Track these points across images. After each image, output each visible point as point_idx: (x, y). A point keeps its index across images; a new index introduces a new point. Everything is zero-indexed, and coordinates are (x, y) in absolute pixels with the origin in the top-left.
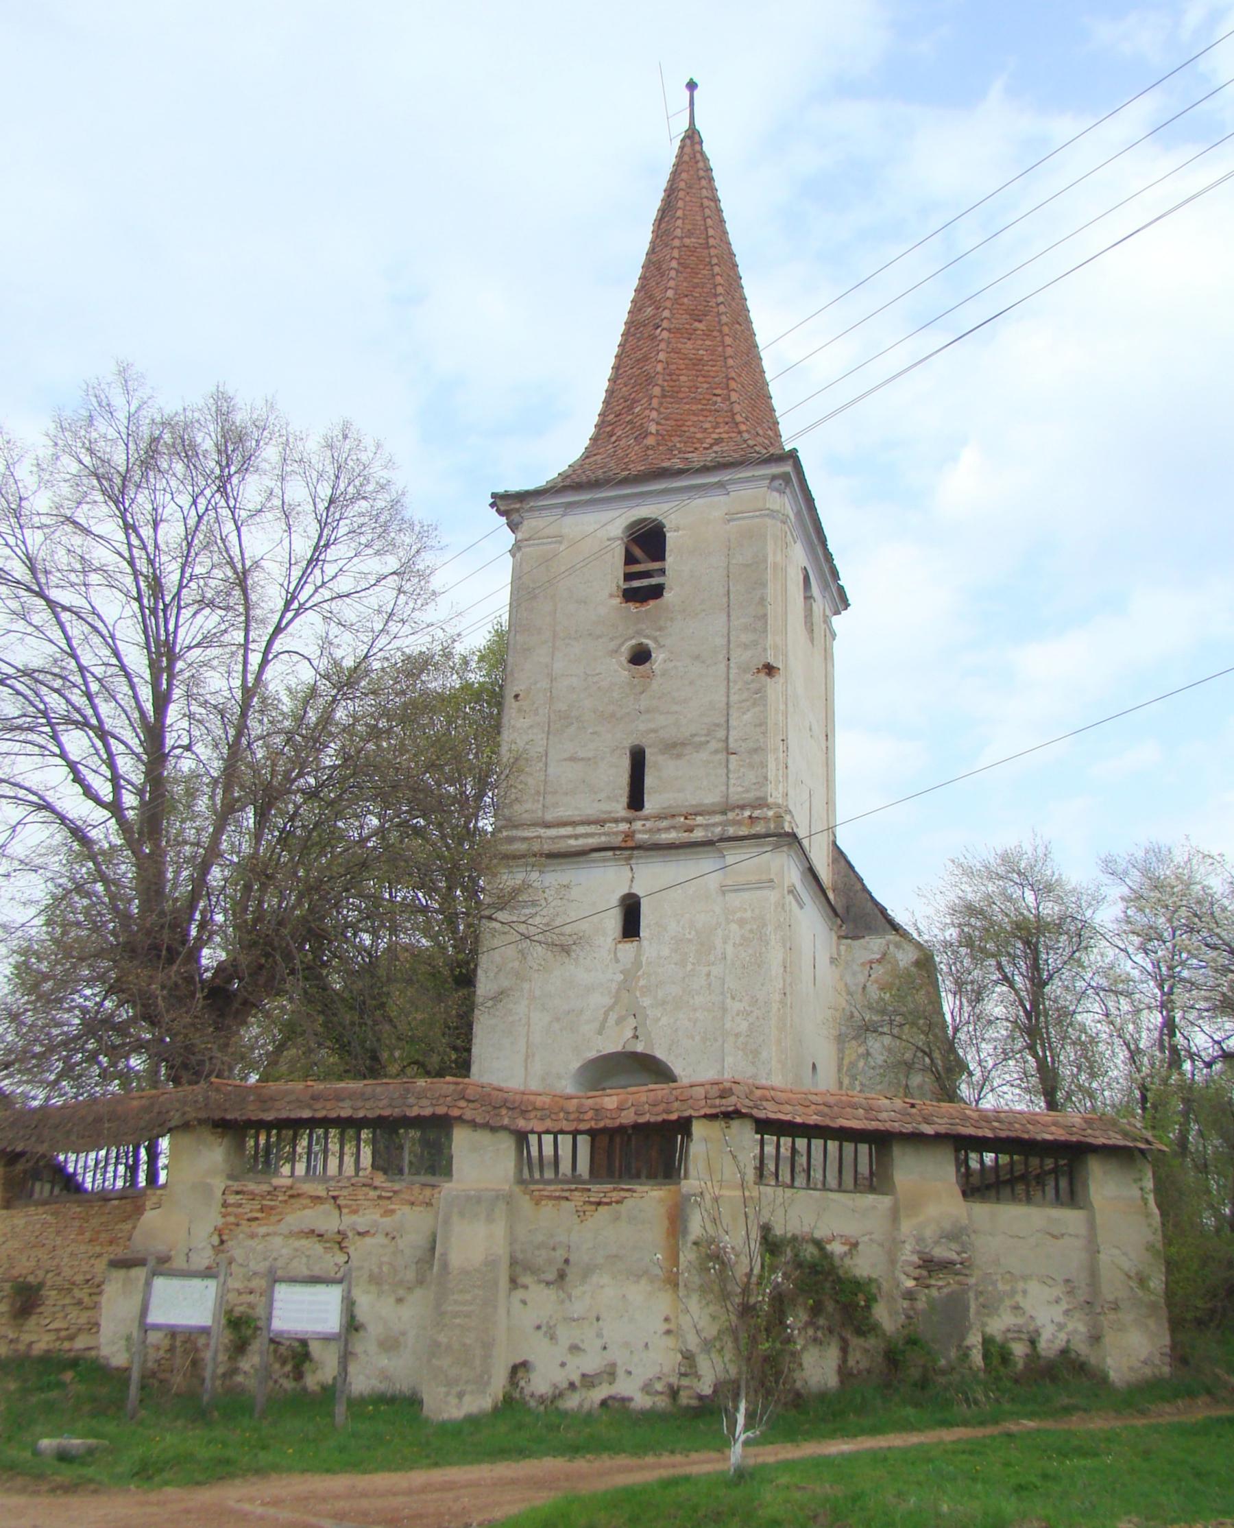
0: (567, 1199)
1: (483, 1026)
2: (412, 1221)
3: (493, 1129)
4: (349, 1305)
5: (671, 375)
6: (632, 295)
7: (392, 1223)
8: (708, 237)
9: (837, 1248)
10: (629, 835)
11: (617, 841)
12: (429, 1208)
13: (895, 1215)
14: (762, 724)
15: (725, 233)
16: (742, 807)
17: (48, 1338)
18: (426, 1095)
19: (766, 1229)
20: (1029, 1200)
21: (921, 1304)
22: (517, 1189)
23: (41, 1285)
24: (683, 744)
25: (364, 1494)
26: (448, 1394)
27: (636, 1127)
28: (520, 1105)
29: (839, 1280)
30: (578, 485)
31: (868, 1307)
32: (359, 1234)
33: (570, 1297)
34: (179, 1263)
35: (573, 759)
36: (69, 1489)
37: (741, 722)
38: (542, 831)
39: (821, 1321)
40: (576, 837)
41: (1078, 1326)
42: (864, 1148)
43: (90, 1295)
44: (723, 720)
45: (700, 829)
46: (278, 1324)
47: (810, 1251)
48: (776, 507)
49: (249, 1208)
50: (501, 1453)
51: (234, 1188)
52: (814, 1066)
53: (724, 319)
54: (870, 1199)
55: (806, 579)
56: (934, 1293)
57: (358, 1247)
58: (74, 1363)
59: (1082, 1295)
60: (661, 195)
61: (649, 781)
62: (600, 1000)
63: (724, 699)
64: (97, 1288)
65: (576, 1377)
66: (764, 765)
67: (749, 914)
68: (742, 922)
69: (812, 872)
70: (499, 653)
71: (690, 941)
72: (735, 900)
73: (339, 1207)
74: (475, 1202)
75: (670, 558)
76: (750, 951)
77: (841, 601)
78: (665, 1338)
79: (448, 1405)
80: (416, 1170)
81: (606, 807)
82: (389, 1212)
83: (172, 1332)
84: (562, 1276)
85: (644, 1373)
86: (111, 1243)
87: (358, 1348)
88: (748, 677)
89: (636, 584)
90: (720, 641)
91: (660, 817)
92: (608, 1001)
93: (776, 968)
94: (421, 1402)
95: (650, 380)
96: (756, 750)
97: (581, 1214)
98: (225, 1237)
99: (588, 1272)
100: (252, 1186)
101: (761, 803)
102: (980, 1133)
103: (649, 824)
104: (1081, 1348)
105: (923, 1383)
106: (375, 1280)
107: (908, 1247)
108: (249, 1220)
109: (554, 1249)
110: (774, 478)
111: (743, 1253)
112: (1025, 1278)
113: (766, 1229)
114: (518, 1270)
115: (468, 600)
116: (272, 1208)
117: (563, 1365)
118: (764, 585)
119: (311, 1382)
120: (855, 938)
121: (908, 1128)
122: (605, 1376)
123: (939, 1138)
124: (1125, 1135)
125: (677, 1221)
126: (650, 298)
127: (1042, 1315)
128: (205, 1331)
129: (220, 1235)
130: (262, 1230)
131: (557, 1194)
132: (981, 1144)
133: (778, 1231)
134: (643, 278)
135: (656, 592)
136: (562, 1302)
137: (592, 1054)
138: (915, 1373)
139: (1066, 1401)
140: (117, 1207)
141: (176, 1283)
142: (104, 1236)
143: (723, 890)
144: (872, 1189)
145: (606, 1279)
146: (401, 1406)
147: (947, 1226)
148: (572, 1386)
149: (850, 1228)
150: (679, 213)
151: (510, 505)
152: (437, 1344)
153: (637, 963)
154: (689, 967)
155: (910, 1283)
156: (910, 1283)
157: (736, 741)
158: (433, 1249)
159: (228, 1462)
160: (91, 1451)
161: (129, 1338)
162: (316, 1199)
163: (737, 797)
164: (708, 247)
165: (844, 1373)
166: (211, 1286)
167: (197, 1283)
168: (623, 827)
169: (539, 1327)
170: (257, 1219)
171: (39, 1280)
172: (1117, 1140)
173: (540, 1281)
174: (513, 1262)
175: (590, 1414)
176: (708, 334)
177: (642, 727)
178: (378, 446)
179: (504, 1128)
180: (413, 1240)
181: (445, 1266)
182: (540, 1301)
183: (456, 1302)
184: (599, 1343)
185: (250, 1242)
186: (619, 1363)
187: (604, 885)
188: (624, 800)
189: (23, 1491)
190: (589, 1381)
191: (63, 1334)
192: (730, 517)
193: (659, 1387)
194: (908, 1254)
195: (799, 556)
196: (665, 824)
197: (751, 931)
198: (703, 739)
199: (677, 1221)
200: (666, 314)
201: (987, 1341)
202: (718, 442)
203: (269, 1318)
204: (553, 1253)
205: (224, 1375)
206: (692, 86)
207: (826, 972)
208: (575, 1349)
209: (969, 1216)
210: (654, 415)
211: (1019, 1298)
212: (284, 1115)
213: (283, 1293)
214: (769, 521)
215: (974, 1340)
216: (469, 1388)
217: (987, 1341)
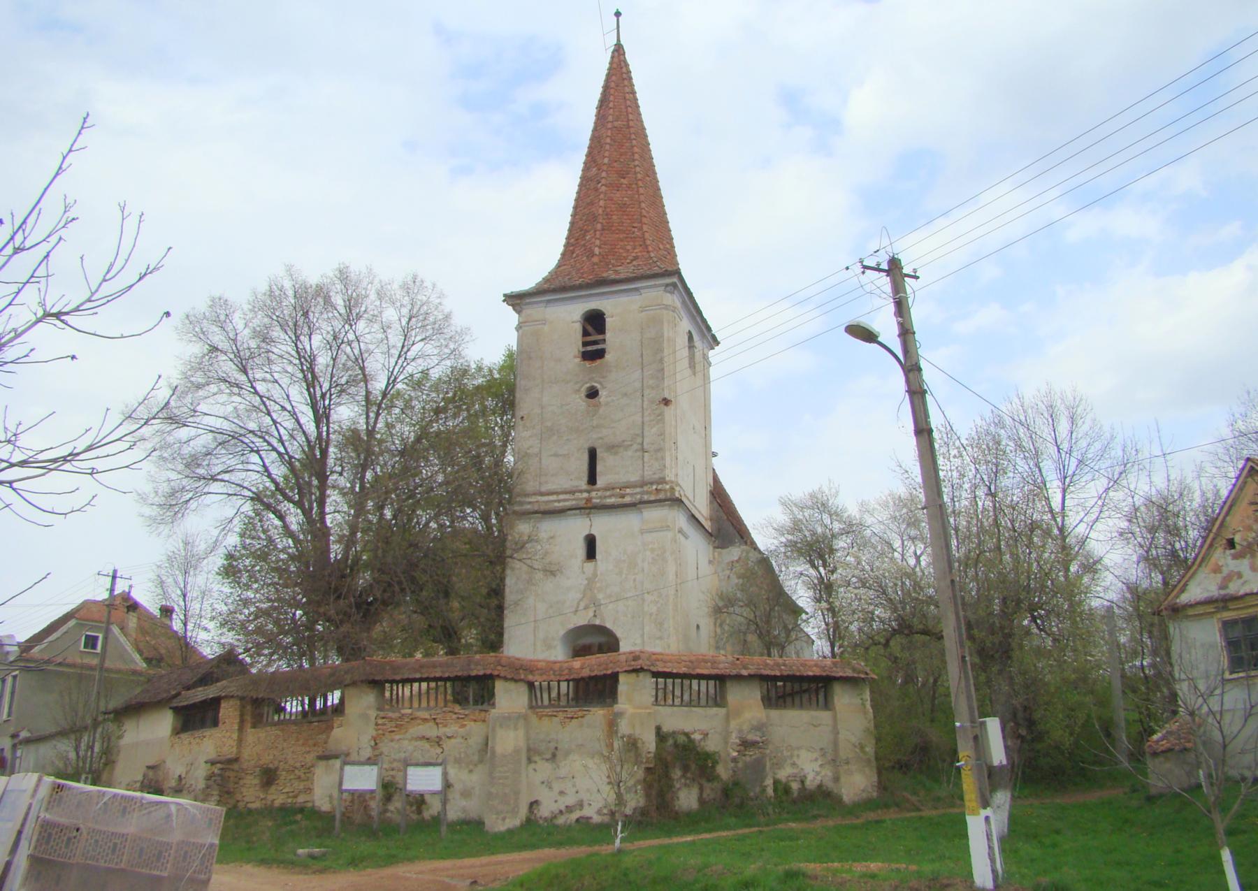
1: (510, 621)
2: (475, 730)
3: (516, 681)
4: (445, 774)
5: (608, 215)
6: (584, 158)
7: (463, 730)
8: (628, 121)
9: (697, 737)
10: (589, 500)
11: (582, 503)
13: (727, 718)
14: (662, 434)
15: (640, 114)
16: (652, 483)
18: (480, 663)
19: (658, 729)
20: (801, 707)
21: (740, 765)
22: (529, 712)
23: (277, 769)
25: (461, 868)
27: (591, 678)
28: (529, 667)
29: (698, 753)
30: (554, 288)
31: (713, 767)
34: (354, 757)
35: (556, 455)
36: (322, 871)
37: (651, 433)
38: (539, 498)
39: (689, 775)
40: (559, 501)
41: (827, 773)
42: (712, 683)
46: (410, 787)
47: (682, 739)
48: (670, 303)
50: (524, 847)
52: (698, 627)
53: (639, 176)
54: (715, 710)
55: (691, 338)
56: (748, 759)
57: (448, 745)
58: (301, 810)
59: (829, 757)
60: (601, 90)
61: (599, 468)
62: (574, 596)
64: (309, 769)
65: (563, 808)
66: (663, 458)
68: (652, 550)
69: (693, 518)
70: (512, 363)
72: (648, 537)
74: (507, 720)
75: (608, 335)
77: (715, 342)
79: (498, 824)
80: (476, 702)
81: (575, 483)
82: (463, 726)
83: (352, 793)
84: (554, 756)
87: (450, 796)
89: (589, 348)
90: (638, 385)
91: (606, 489)
92: (579, 596)
93: (671, 576)
94: (484, 823)
95: (594, 218)
97: (563, 724)
99: (567, 753)
100: (390, 714)
101: (662, 481)
102: (773, 673)
103: (600, 493)
104: (829, 784)
105: (741, 806)
106: (458, 761)
107: (734, 735)
110: (667, 285)
111: (649, 743)
112: (799, 748)
113: (658, 729)
114: (532, 754)
115: (490, 340)
118: (662, 351)
119: (427, 815)
120: (722, 548)
121: (734, 672)
123: (750, 676)
124: (854, 670)
125: (612, 725)
126: (595, 161)
127: (810, 768)
128: (372, 791)
130: (397, 737)
132: (774, 678)
133: (665, 729)
134: (590, 147)
135: (600, 354)
137: (571, 626)
138: (737, 801)
139: (816, 812)
141: (356, 768)
142: (311, 742)
143: (642, 532)
144: (717, 705)
146: (473, 826)
147: (755, 723)
149: (704, 726)
150: (611, 105)
151: (516, 300)
153: (595, 575)
155: (735, 754)
156: (735, 754)
158: (487, 744)
159: (394, 856)
160: (324, 855)
161: (331, 797)
162: (425, 720)
164: (629, 127)
165: (701, 801)
166: (375, 768)
167: (367, 768)
168: (585, 495)
172: (849, 673)
174: (529, 750)
175: (570, 826)
176: (629, 187)
177: (595, 436)
178: (434, 286)
179: (521, 680)
180: (476, 741)
181: (493, 752)
182: (543, 769)
187: (573, 530)
188: (585, 479)
189: (300, 873)
190: (569, 809)
192: (642, 309)
193: (605, 811)
194: (734, 739)
195: (685, 325)
196: (608, 493)
199: (612, 725)
200: (604, 174)
201: (776, 782)
202: (636, 258)
203: (405, 783)
206: (618, 14)
207: (705, 569)
208: (562, 793)
209: (768, 717)
210: (598, 242)
211: (795, 759)
212: (406, 676)
213: (411, 771)
214: (665, 312)
215: (769, 782)
217: (776, 782)
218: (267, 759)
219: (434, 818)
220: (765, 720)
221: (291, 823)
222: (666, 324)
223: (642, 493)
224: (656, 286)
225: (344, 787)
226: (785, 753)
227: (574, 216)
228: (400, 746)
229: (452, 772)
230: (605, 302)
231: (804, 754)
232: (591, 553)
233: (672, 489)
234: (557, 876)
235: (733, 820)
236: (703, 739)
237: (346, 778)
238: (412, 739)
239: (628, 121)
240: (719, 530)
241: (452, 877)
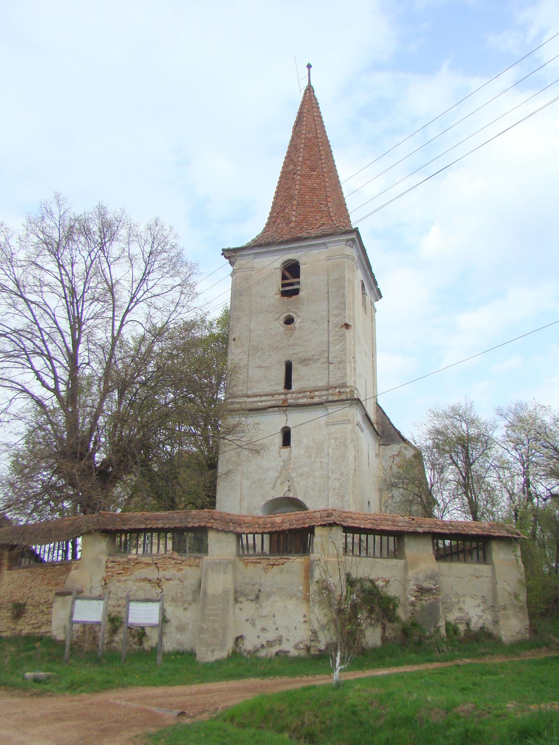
0: (259, 563)
2: (190, 574)
3: (226, 532)
4: (163, 611)
5: (301, 195)
6: (284, 160)
7: (181, 575)
8: (317, 134)
9: (380, 583)
10: (285, 400)
11: (280, 403)
13: (406, 568)
15: (325, 132)
16: (335, 388)
18: (196, 517)
19: (348, 575)
20: (465, 561)
21: (418, 608)
22: (237, 559)
23: (25, 604)
24: (309, 360)
25: (171, 696)
26: (207, 650)
27: (290, 530)
28: (238, 521)
29: (381, 598)
30: (260, 245)
31: (394, 609)
32: (167, 579)
33: (261, 606)
35: (259, 367)
36: (39, 695)
37: (335, 349)
38: (246, 399)
39: (373, 616)
40: (262, 401)
41: (488, 617)
42: (391, 539)
43: (47, 608)
44: (326, 349)
45: (317, 397)
46: (131, 620)
47: (368, 585)
49: (118, 569)
54: (395, 561)
56: (424, 603)
57: (166, 586)
58: (40, 639)
59: (490, 603)
60: (296, 115)
61: (294, 376)
62: (272, 474)
63: (327, 339)
64: (50, 605)
65: (264, 643)
66: (345, 369)
67: (339, 435)
68: (336, 439)
69: (367, 416)
70: (226, 320)
71: (313, 447)
72: (333, 429)
73: (158, 568)
74: (218, 565)
75: (302, 277)
76: (340, 452)
77: (379, 295)
78: (304, 624)
80: (192, 551)
81: (274, 388)
82: (180, 570)
83: (84, 624)
84: (257, 597)
85: (294, 640)
86: (56, 585)
87: (167, 630)
88: (338, 329)
89: (287, 288)
91: (299, 392)
92: (277, 474)
94: (195, 654)
95: (292, 197)
96: (341, 362)
97: (266, 570)
98: (107, 582)
99: (269, 595)
100: (119, 559)
101: (344, 385)
102: (443, 531)
103: (294, 396)
104: (490, 627)
105: (419, 643)
106: (174, 600)
108: (117, 574)
109: (254, 585)
110: (348, 241)
112: (464, 596)
113: (348, 575)
114: (238, 595)
115: (212, 297)
116: (128, 568)
117: (258, 637)
118: (344, 288)
119: (147, 645)
120: (387, 445)
121: (411, 530)
122: (277, 641)
123: (424, 533)
124: (508, 531)
125: (308, 572)
126: (292, 161)
127: (471, 611)
128: (98, 623)
129: (105, 581)
130: (124, 578)
132: (444, 536)
133: (354, 576)
134: (288, 152)
135: (296, 292)
136: (258, 609)
137: (270, 498)
138: (415, 639)
140: (59, 569)
141: (85, 602)
142: (53, 582)
143: (328, 424)
144: (395, 557)
145: (277, 599)
146: (186, 656)
148: (263, 646)
149: (386, 574)
150: (304, 123)
151: (230, 254)
153: (289, 458)
154: (313, 459)
155: (413, 599)
156: (413, 599)
157: (332, 358)
158: (200, 586)
159: (110, 682)
160: (48, 678)
161: (65, 627)
162: (148, 564)
163: (333, 383)
164: (317, 138)
165: (384, 639)
166: (102, 603)
167: (95, 602)
168: (283, 397)
170: (121, 573)
171: (24, 602)
173: (248, 600)
174: (236, 591)
175: (270, 658)
176: (318, 177)
177: (290, 352)
179: (231, 532)
180: (191, 582)
181: (205, 593)
182: (248, 608)
183: (211, 609)
186: (284, 636)
187: (274, 423)
188: (283, 385)
189: (18, 696)
190: (270, 644)
192: (329, 258)
193: (301, 646)
194: (412, 586)
195: (359, 275)
196: (301, 395)
197: (340, 442)
198: (318, 357)
199: (308, 572)
200: (299, 168)
201: (448, 624)
202: (323, 225)
206: (309, 66)
208: (264, 629)
211: (461, 604)
212: (133, 527)
213: (133, 606)
214: (346, 260)
215: (442, 623)
217: (448, 624)
218: (18, 596)
219: (152, 648)
220: (437, 571)
221: (29, 649)
222: (347, 269)
223: (327, 395)
224: (339, 241)
225: (75, 618)
226: (453, 600)
227: (275, 198)
228: (129, 584)
229: (166, 606)
230: (300, 254)
231: (468, 600)
232: (286, 440)
233: (352, 392)
234: (272, 711)
235: (413, 655)
236: (386, 586)
237: (76, 611)
238: (137, 580)
239: (317, 134)
240: (383, 432)
241: (160, 706)
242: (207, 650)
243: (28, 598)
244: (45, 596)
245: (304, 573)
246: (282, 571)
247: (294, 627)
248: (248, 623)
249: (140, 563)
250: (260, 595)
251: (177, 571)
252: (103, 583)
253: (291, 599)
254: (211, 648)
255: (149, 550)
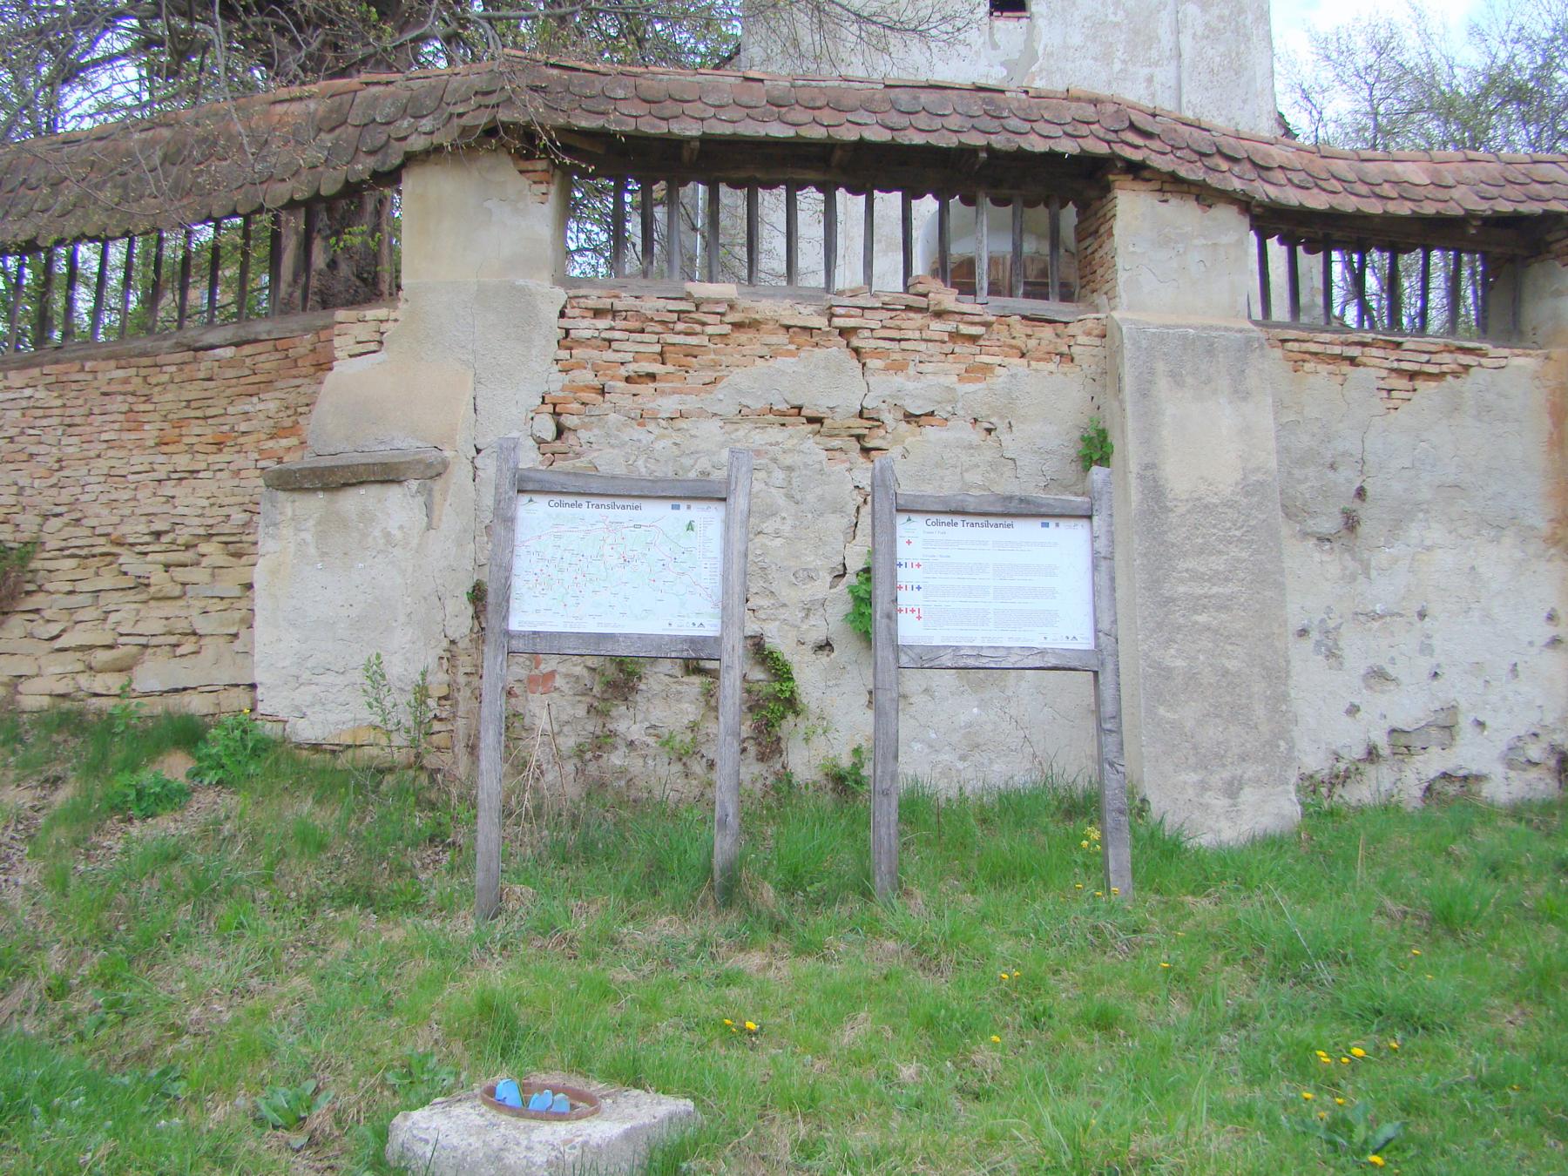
0: (1352, 361)
12: (1066, 367)
17: (55, 666)
26: (1203, 786)
32: (909, 417)
33: (1366, 569)
43: (167, 567)
49: (635, 352)
51: (591, 303)
71: (1116, 25)
73: (856, 351)
76: (1222, 49)
78: (1549, 654)
84: (1351, 523)
85: (1507, 726)
86: (219, 445)
98: (568, 421)
108: (628, 379)
109: (1332, 467)
117: (1353, 710)
122: (1434, 732)
129: (556, 414)
130: (668, 405)
131: (1337, 350)
136: (1353, 578)
140: (230, 363)
145: (1436, 534)
148: (1372, 754)
152: (1166, 673)
154: (1117, 66)
166: (709, 517)
169: (1303, 633)
170: (652, 377)
171: (26, 536)
173: (1305, 535)
181: (1155, 491)
183: (1197, 577)
184: (1425, 664)
185: (638, 433)
186: (1463, 704)
190: (1403, 743)
191: (102, 656)
197: (1221, 18)
204: (1331, 474)
205: (580, 752)
208: (1378, 676)
216: (1252, 770)
242: (1203, 786)
243: (46, 517)
244: (148, 503)
245: (1547, 423)
246: (1456, 408)
247: (1507, 667)
248: (1308, 644)
249: (754, 325)
250: (1364, 511)
251: (960, 378)
252: (547, 429)
253: (1496, 540)
254: (1218, 778)
255: (810, 256)
